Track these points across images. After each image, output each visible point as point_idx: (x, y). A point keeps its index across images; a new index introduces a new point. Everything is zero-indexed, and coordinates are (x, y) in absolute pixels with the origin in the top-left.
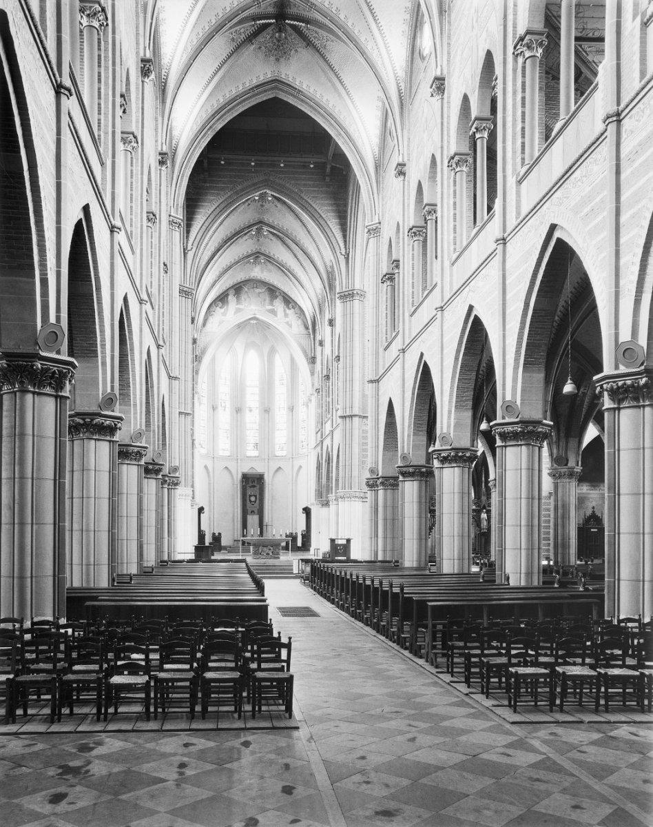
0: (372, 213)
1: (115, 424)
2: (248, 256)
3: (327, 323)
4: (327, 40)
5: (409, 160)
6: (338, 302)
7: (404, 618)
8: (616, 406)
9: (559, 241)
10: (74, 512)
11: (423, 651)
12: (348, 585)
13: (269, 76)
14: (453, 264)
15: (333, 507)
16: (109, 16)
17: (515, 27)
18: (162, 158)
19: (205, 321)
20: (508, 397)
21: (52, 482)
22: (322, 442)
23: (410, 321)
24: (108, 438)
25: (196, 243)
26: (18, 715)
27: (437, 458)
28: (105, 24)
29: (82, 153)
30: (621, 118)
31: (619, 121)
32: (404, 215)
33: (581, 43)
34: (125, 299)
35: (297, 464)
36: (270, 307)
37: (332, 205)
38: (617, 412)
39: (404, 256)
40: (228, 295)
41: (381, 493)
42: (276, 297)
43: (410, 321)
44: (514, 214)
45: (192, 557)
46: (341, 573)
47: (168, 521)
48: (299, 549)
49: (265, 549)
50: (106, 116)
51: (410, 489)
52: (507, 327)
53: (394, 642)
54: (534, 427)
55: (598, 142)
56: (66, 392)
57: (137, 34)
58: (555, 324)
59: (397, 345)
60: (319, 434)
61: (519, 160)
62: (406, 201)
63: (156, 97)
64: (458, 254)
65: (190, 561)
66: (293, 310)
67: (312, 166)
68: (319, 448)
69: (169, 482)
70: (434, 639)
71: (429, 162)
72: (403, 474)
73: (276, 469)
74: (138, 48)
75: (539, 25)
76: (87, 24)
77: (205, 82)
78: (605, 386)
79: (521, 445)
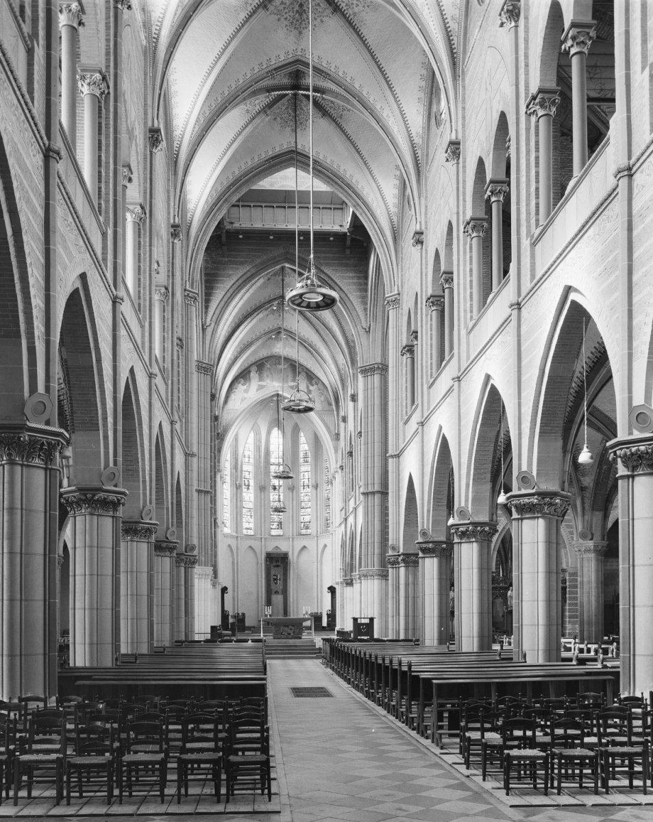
0: (391, 284)
1: (118, 500)
2: (271, 331)
3: (349, 398)
4: (344, 110)
5: (426, 228)
6: (360, 376)
7: (412, 699)
8: (629, 473)
9: (574, 303)
10: (77, 590)
11: (429, 732)
12: (362, 662)
13: (285, 147)
14: (470, 333)
15: (357, 586)
16: (111, 85)
17: (527, 87)
19: (227, 397)
20: (524, 468)
21: (42, 557)
22: (346, 519)
23: (429, 394)
25: (214, 318)
26: (21, 798)
27: (456, 532)
28: (106, 92)
29: (77, 220)
30: (633, 172)
31: (631, 176)
32: (422, 285)
33: (599, 104)
34: (132, 371)
36: (292, 384)
37: (353, 278)
38: (631, 480)
39: (422, 326)
40: (250, 372)
41: (402, 570)
43: (429, 394)
44: (529, 277)
45: (209, 637)
46: (356, 652)
47: (185, 602)
48: (324, 629)
50: (107, 182)
51: (430, 566)
52: (523, 395)
53: (403, 722)
54: (551, 499)
55: (611, 198)
56: (56, 465)
57: (146, 105)
58: (572, 391)
59: (416, 418)
60: (343, 511)
61: (533, 221)
62: (424, 270)
63: (168, 169)
64: (474, 322)
65: (207, 641)
67: (331, 239)
68: (343, 526)
69: (185, 560)
70: (440, 718)
71: (446, 229)
72: (424, 551)
74: (146, 118)
75: (552, 84)
76: (88, 92)
77: (219, 154)
78: (618, 452)
79: (538, 518)
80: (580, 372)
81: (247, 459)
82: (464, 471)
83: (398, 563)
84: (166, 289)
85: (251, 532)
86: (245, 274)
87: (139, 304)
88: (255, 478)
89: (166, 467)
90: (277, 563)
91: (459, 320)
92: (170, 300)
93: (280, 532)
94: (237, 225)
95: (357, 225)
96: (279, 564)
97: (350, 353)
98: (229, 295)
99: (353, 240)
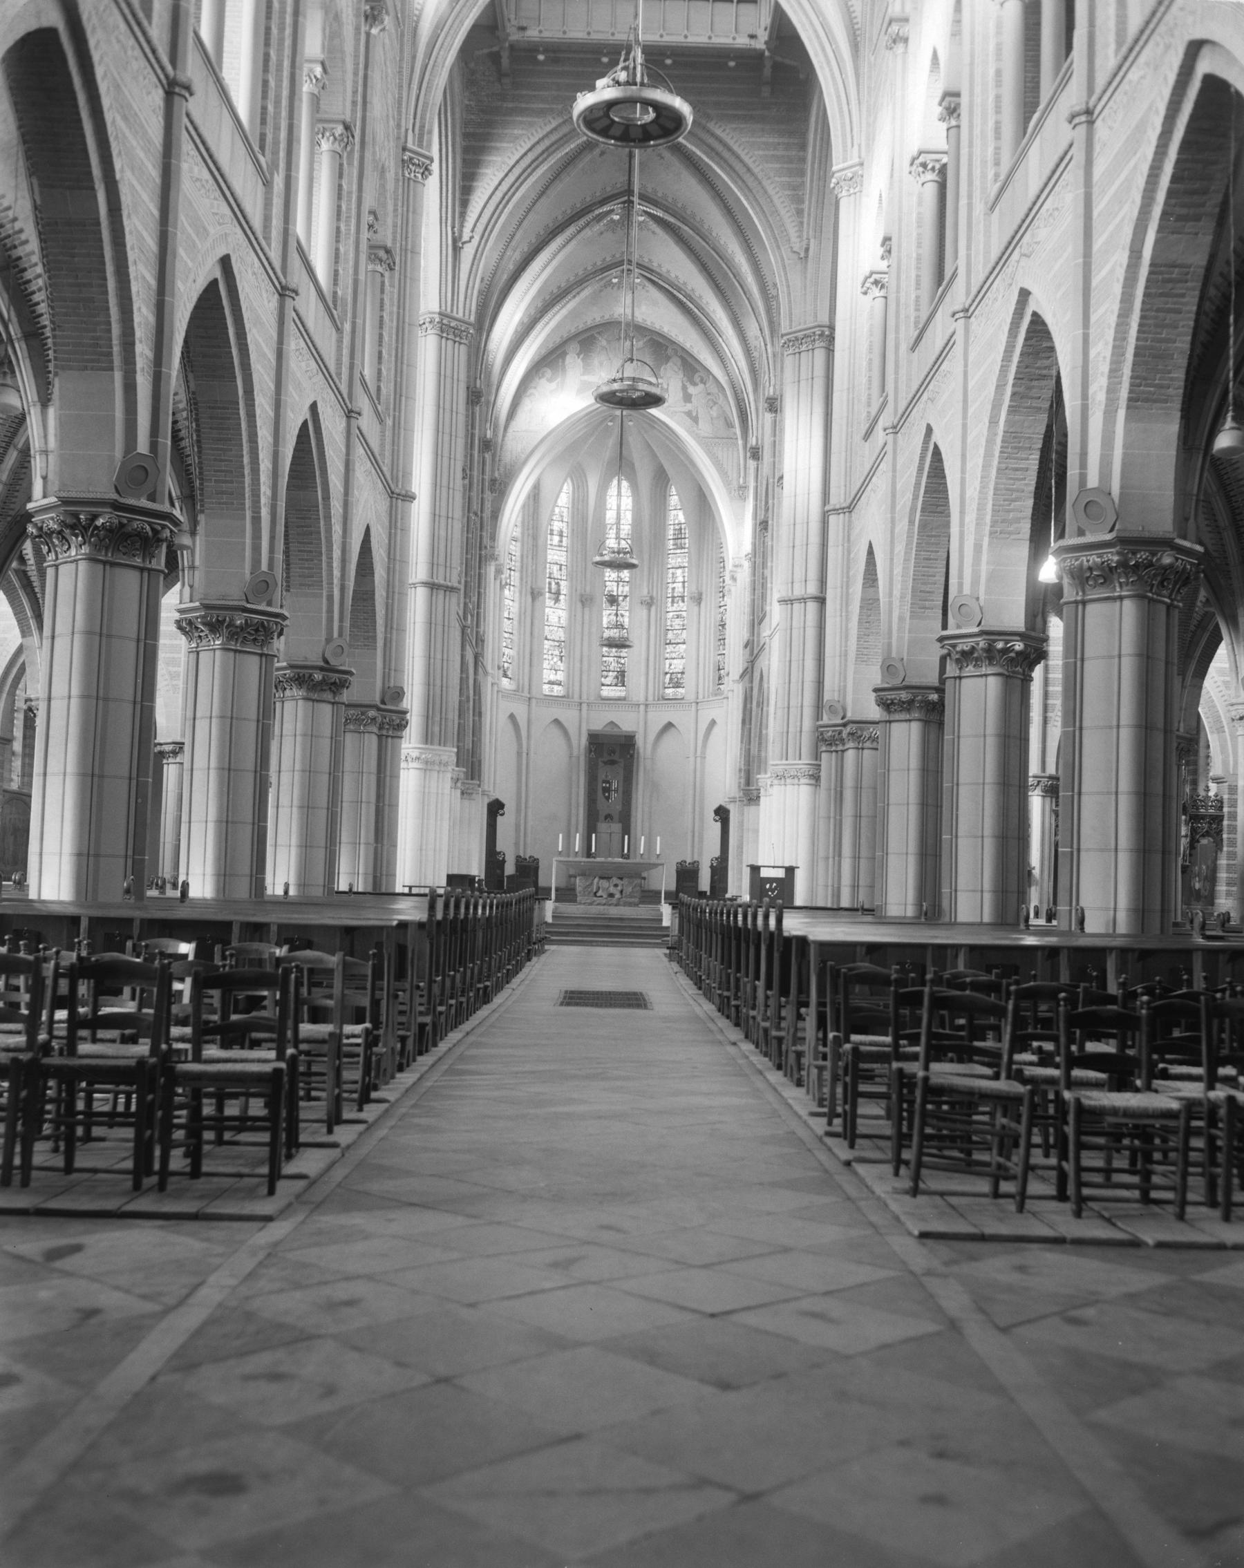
1: (153, 529)
14: (992, 208)
18: (372, 8)
24: (138, 561)
35: (706, 715)
42: (668, 359)
49: (604, 883)
52: (1093, 318)
66: (701, 386)
73: (660, 727)
79: (1121, 598)
80: (1221, 274)
81: (556, 539)
82: (971, 518)
83: (842, 741)
84: (347, 127)
85: (558, 691)
86: (546, 136)
87: (263, 138)
88: (571, 577)
89: (327, 507)
90: (611, 760)
91: (970, 183)
92: (356, 155)
93: (617, 692)
94: (533, 34)
95: (784, 35)
96: (616, 757)
97: (769, 310)
98: (511, 178)
99: (776, 67)
